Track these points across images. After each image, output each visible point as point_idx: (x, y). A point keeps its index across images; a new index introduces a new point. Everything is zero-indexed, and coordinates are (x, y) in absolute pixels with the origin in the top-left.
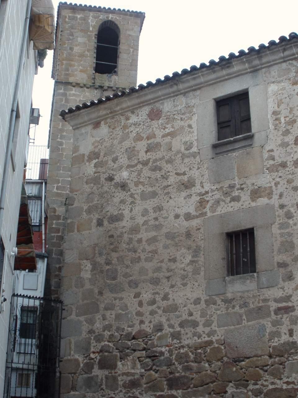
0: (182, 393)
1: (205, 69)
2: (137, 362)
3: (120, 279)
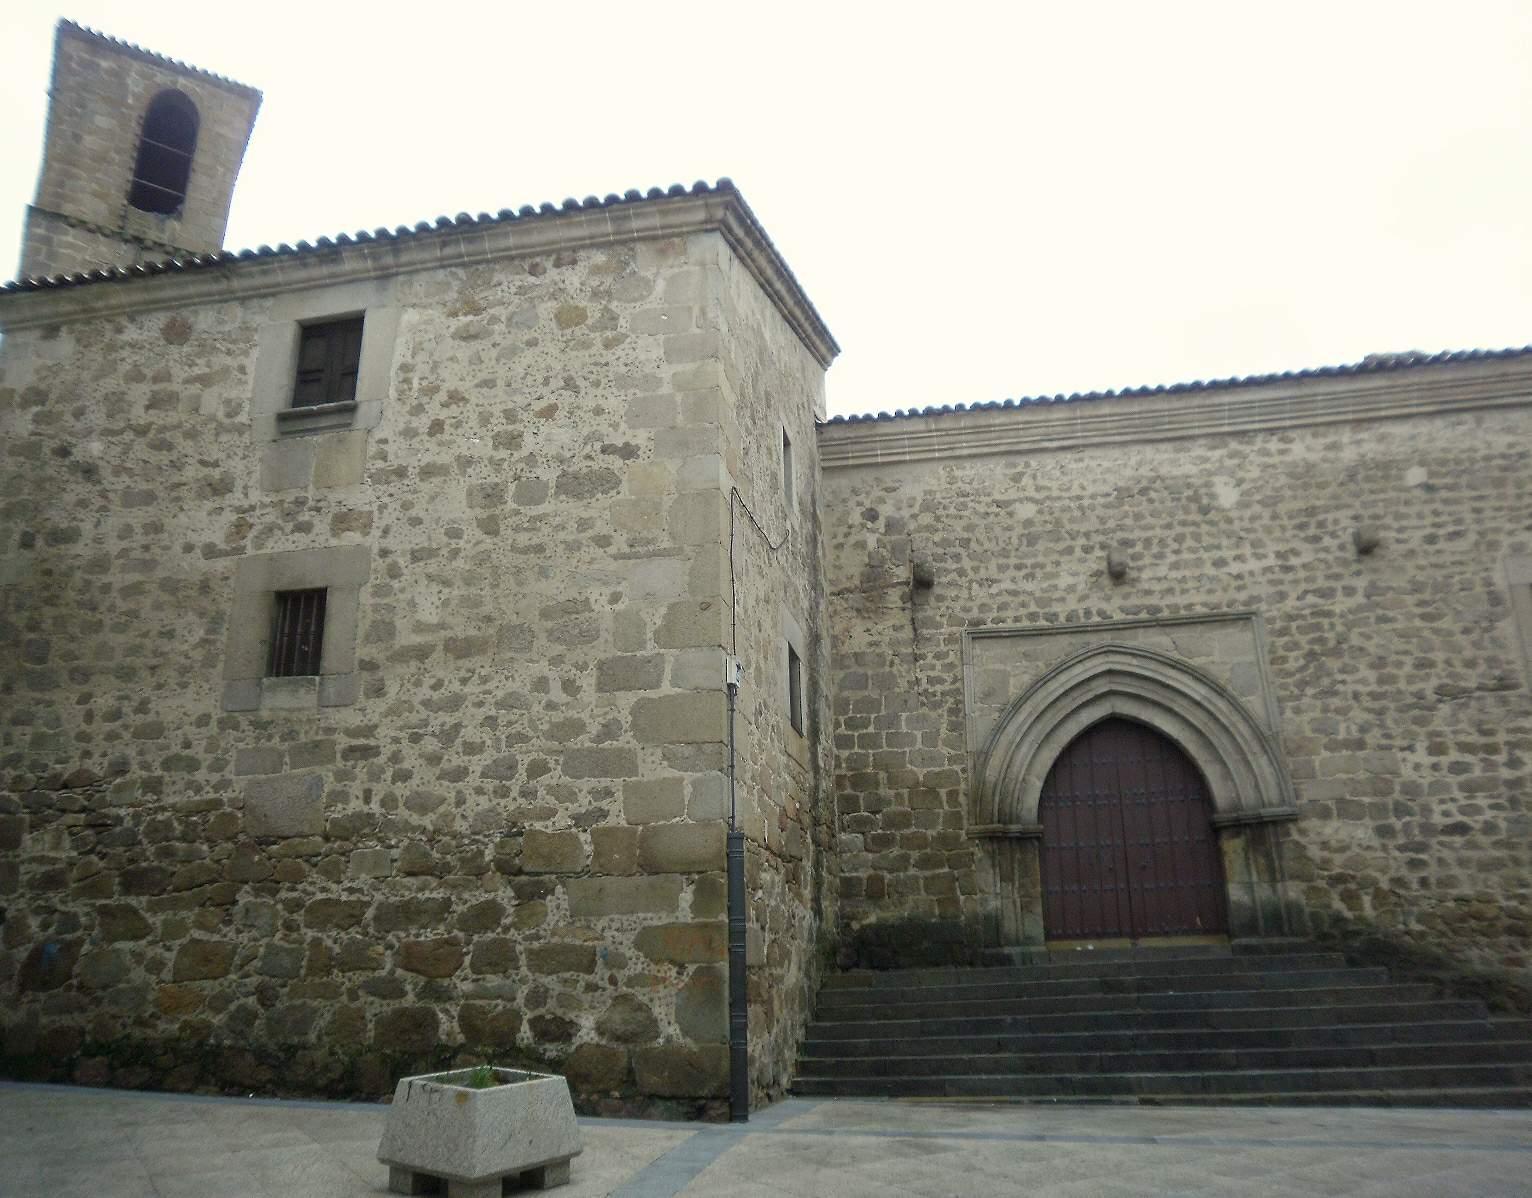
0: (149, 902)
1: (615, 206)
2: (66, 836)
3: (55, 662)
